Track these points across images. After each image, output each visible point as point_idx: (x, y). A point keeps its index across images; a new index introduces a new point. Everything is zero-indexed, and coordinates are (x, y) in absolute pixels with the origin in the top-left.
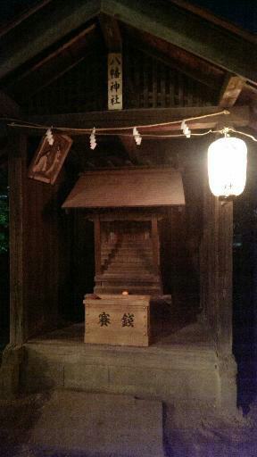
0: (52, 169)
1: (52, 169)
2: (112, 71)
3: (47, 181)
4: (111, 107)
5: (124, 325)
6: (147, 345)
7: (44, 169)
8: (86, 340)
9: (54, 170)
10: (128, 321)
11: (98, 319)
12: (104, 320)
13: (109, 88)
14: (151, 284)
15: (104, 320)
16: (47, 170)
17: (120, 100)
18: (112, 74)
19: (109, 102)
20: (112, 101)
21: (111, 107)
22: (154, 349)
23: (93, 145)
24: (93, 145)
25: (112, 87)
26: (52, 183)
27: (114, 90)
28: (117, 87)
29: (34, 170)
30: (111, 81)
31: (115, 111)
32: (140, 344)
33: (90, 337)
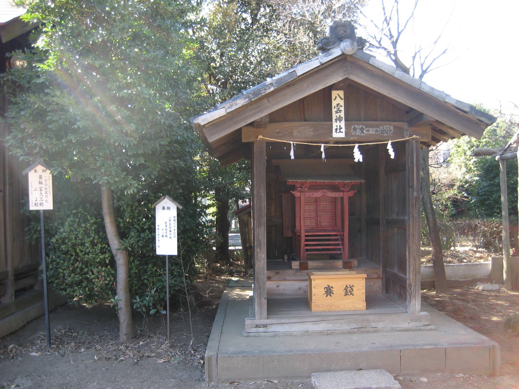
5: (346, 294)
12: (329, 291)
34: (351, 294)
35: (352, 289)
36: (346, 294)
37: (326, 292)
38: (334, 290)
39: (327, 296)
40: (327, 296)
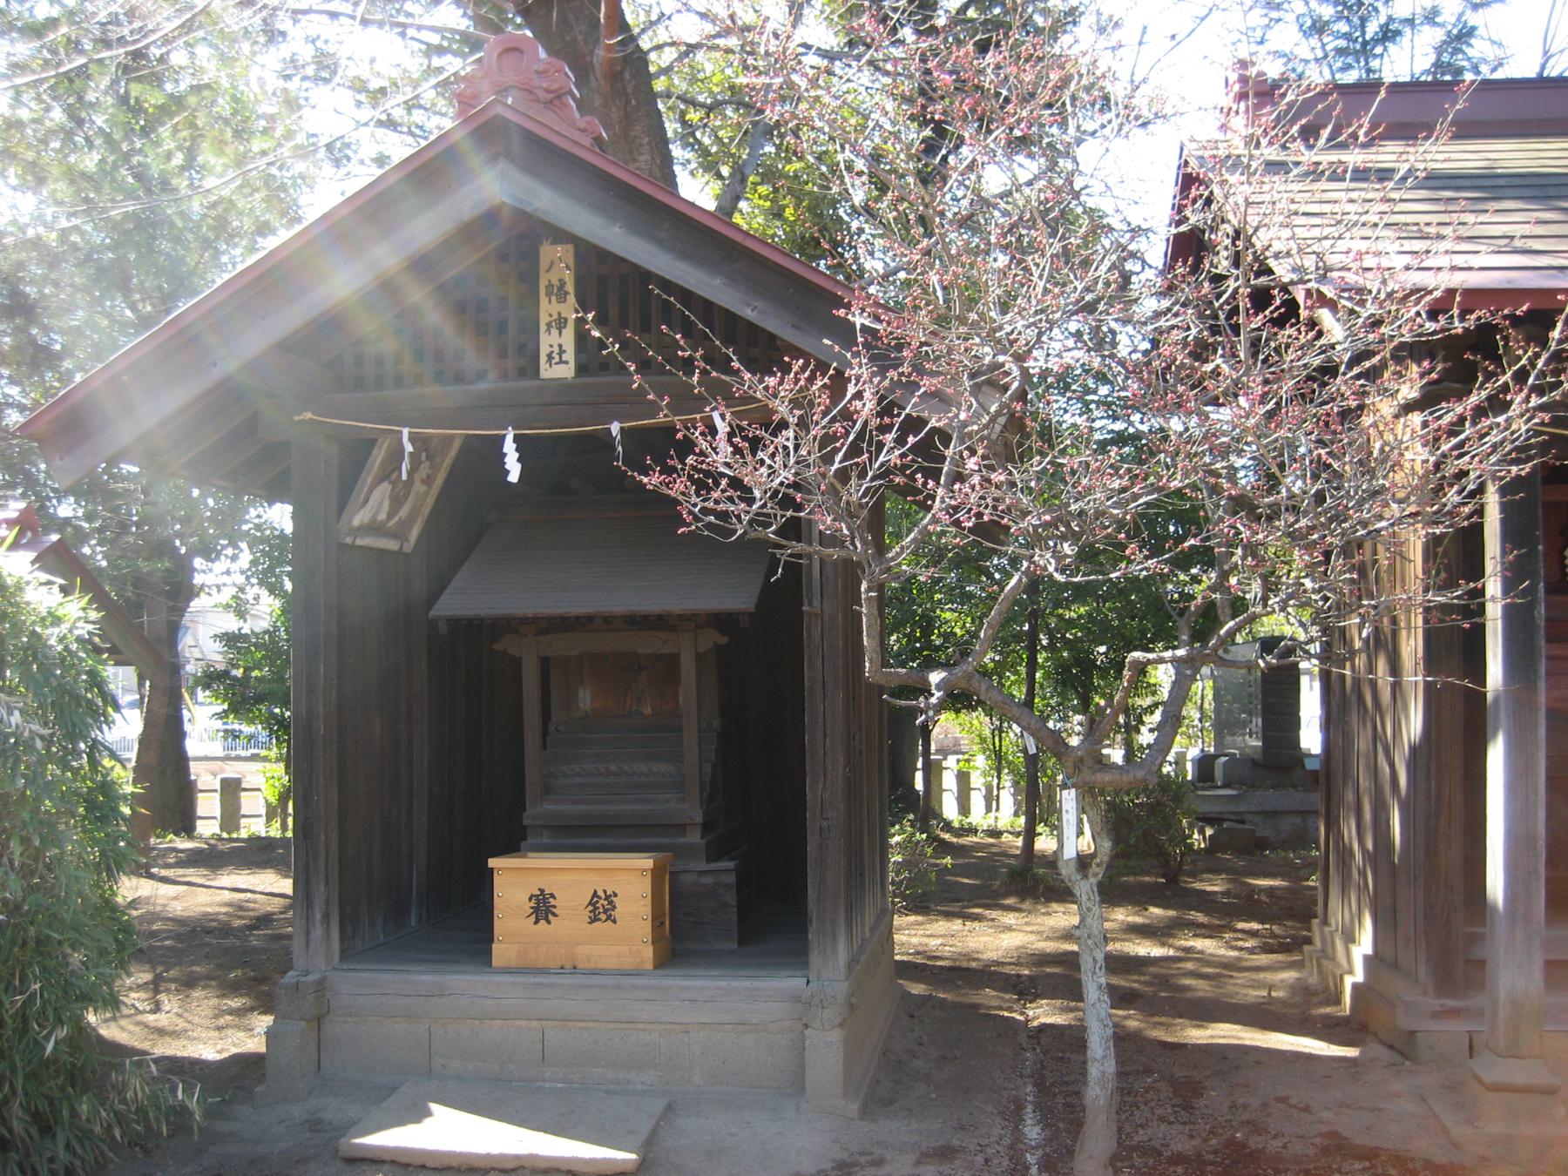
0: (403, 512)
1: (403, 512)
2: (550, 285)
3: (392, 545)
4: (548, 372)
5: (594, 920)
6: (649, 965)
7: (382, 516)
8: (496, 962)
9: (1136, 982)
10: (601, 908)
11: (527, 907)
12: (543, 908)
13: (543, 328)
14: (681, 828)
15: (543, 908)
16: (391, 515)
17: (570, 355)
18: (549, 294)
19: (543, 359)
20: (550, 357)
21: (548, 372)
22: (659, 972)
23: (514, 470)
24: (514, 470)
25: (549, 325)
26: (408, 548)
27: (554, 332)
28: (561, 323)
29: (356, 522)
30: (548, 309)
31: (560, 384)
32: (628, 963)
33: (502, 952)
34: (609, 917)
35: (611, 903)
36: (594, 920)
37: (536, 910)
38: (560, 903)
39: (536, 922)
40: (536, 922)
